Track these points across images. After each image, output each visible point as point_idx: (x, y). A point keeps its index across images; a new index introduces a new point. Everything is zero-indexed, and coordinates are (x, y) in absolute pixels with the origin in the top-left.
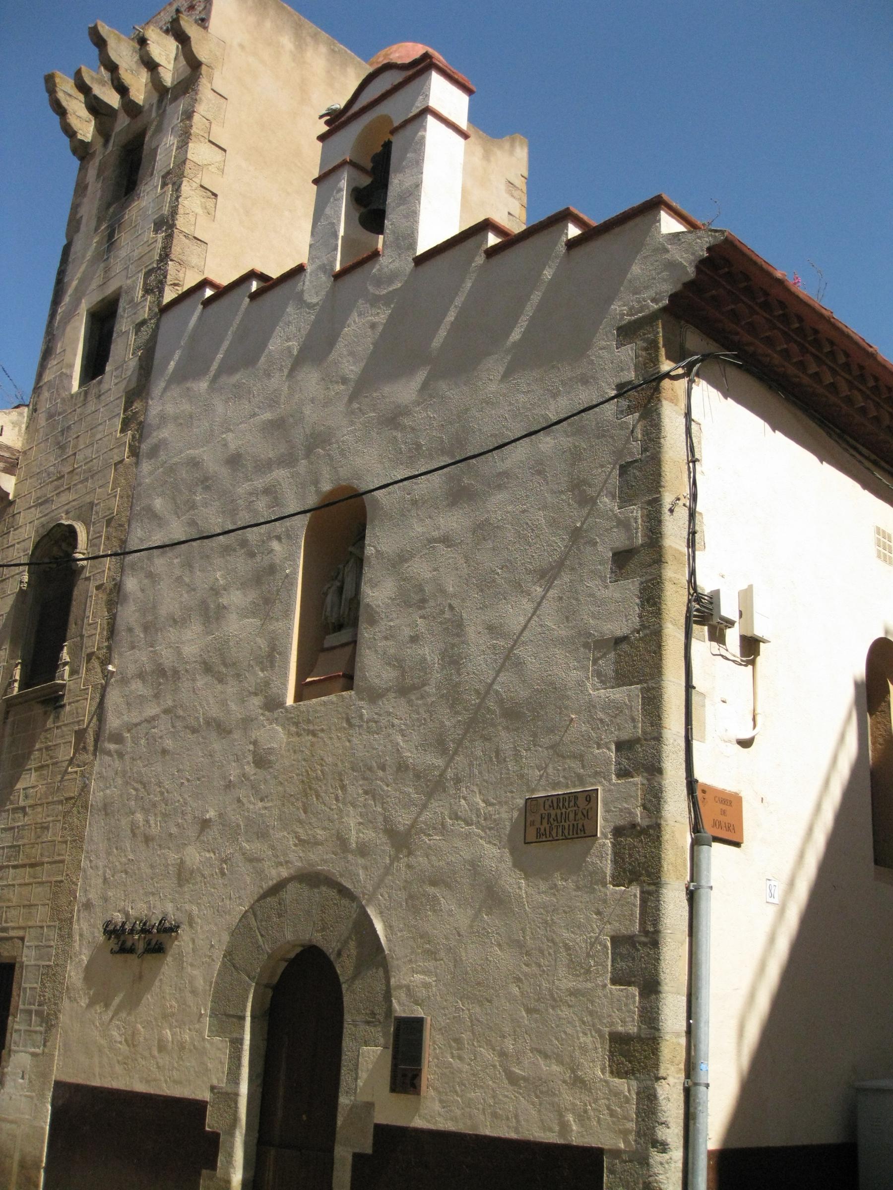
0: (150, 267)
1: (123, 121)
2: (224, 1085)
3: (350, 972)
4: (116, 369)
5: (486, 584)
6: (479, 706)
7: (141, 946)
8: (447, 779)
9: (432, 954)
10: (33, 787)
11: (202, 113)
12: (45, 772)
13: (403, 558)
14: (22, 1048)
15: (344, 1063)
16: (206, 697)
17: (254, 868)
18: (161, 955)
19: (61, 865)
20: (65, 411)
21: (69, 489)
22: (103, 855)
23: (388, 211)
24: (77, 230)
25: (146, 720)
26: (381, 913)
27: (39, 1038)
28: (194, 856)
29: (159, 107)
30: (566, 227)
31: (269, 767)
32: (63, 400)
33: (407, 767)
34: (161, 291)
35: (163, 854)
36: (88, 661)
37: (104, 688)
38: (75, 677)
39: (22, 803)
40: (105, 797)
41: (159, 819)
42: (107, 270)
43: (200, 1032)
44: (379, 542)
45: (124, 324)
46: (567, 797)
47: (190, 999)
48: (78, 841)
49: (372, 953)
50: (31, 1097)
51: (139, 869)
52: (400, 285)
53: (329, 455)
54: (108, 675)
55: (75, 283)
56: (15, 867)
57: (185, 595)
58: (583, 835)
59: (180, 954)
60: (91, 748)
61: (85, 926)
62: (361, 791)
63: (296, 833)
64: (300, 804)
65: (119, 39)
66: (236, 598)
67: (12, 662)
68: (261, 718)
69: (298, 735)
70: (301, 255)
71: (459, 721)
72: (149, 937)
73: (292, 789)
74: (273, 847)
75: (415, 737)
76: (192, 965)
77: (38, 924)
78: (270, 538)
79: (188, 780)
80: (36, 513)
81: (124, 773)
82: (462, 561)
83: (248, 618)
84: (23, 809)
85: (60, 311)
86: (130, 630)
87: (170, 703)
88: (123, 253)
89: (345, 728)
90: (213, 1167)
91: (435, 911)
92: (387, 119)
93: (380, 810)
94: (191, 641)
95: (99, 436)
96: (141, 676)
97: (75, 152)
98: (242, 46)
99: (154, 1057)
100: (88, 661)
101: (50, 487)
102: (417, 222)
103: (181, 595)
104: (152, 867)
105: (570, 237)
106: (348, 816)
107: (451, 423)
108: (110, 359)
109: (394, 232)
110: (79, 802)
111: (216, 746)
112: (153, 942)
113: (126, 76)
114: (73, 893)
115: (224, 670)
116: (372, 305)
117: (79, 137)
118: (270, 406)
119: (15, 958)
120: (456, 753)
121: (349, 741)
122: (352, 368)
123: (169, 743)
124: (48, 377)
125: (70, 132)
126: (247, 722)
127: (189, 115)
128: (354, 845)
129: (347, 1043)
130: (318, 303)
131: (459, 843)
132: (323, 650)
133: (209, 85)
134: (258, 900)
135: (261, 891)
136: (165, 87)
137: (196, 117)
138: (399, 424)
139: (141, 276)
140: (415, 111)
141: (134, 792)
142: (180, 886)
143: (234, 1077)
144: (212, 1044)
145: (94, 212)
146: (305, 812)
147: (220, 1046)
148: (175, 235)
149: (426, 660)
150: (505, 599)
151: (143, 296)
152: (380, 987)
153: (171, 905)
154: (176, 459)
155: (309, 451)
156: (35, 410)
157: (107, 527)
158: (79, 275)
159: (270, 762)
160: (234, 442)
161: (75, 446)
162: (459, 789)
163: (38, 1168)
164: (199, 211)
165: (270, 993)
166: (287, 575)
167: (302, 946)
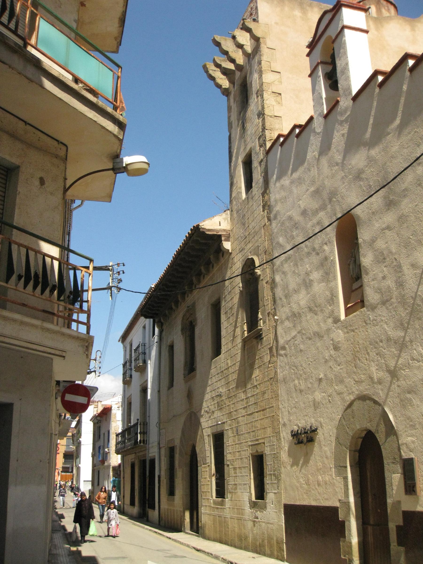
0: (259, 135)
1: (238, 74)
2: (343, 499)
3: (383, 440)
4: (256, 184)
5: (407, 245)
6: (413, 304)
7: (305, 440)
8: (407, 342)
9: (413, 427)
10: (258, 376)
11: (265, 60)
12: (261, 369)
13: (373, 241)
14: (270, 491)
15: (387, 483)
16: (312, 323)
17: (341, 397)
18: (313, 443)
19: (272, 408)
20: (242, 208)
21: (249, 242)
22: (286, 401)
23: (339, 79)
24: (232, 128)
25: (292, 338)
26: (391, 410)
27: (275, 486)
28: (318, 396)
29: (249, 63)
30: (408, 62)
31: (340, 350)
32: (240, 203)
33: (391, 339)
34: (265, 144)
35: (307, 397)
36: (268, 316)
37: (276, 327)
38: (265, 324)
39: (255, 384)
40: (283, 375)
41: (304, 381)
42: (245, 141)
43: (331, 475)
44: (364, 235)
45: (255, 164)
47: (326, 461)
48: (277, 396)
49: (391, 430)
50: (276, 512)
51: (300, 405)
52: (349, 113)
53: (338, 200)
54: (276, 321)
55: (235, 151)
56: (257, 412)
57: (297, 279)
59: (320, 441)
60: (275, 355)
61: (285, 434)
62: (375, 354)
63: (353, 378)
64: (353, 365)
65: (226, 40)
66: (316, 275)
67: (242, 323)
68: (333, 328)
69: (348, 333)
70: (311, 113)
71: (407, 313)
72: (307, 435)
73: (349, 359)
74: (346, 387)
75: (392, 324)
76: (324, 445)
77: (269, 436)
78: (323, 245)
79: (311, 362)
80: (240, 255)
81: (288, 362)
82: (396, 236)
83: (321, 283)
84: (256, 386)
85: (232, 165)
86: (281, 299)
87: (300, 328)
88: (249, 132)
89: (365, 326)
90: (345, 537)
91: (411, 406)
92: (330, 37)
93: (383, 361)
94: (302, 299)
95: (255, 216)
96: (287, 318)
97: (223, 94)
98: (277, 23)
99: (316, 489)
100: (268, 316)
101: (243, 243)
102: (350, 81)
103: (296, 279)
104: (304, 403)
105: (410, 66)
106: (372, 366)
107: (380, 172)
108: (253, 180)
109: (342, 89)
110: (274, 379)
111: (319, 344)
112: (309, 437)
113: (233, 55)
114: (278, 420)
115: (316, 309)
116: (341, 125)
117: (223, 87)
118: (313, 184)
119: (263, 452)
120: (408, 328)
121: (367, 331)
122: (339, 157)
123: (302, 347)
124: (234, 195)
125: (219, 86)
126: (328, 330)
127: (260, 63)
128: (376, 380)
129: (387, 474)
130: (321, 132)
131: (416, 372)
132: (353, 291)
133: (265, 46)
134: (345, 411)
135: (345, 408)
136: (248, 53)
137: (263, 63)
138: (361, 178)
139: (257, 140)
140: (339, 29)
141: (293, 371)
142: (315, 410)
143: (347, 495)
144: (336, 480)
145: (236, 117)
146: (356, 368)
147: (340, 481)
148: (265, 118)
149: (390, 286)
150: (416, 250)
151: (260, 149)
152: (395, 446)
153: (313, 419)
154: (284, 218)
155: (330, 200)
156: (232, 211)
157: (265, 255)
158: (236, 147)
159: (339, 347)
160: (302, 204)
161: (248, 223)
162: (412, 346)
163: (283, 543)
164: (274, 103)
165: (357, 454)
166: (332, 260)
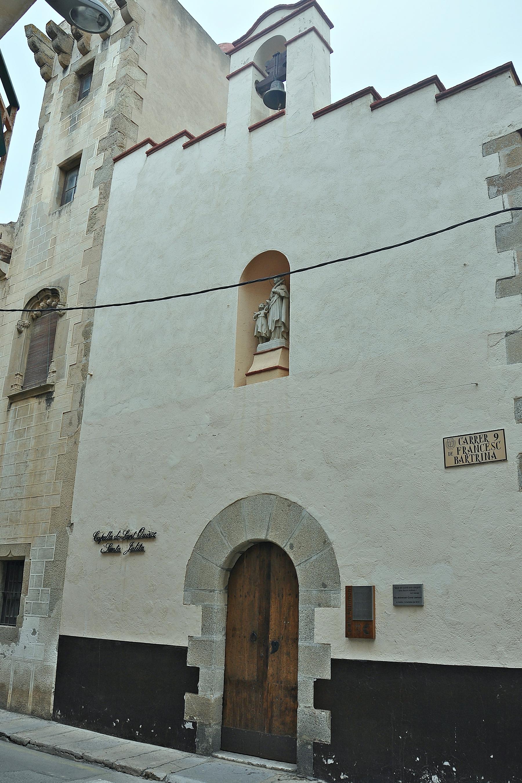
46: (478, 435)
58: (494, 459)
164: (133, 106)
167: (254, 543)
